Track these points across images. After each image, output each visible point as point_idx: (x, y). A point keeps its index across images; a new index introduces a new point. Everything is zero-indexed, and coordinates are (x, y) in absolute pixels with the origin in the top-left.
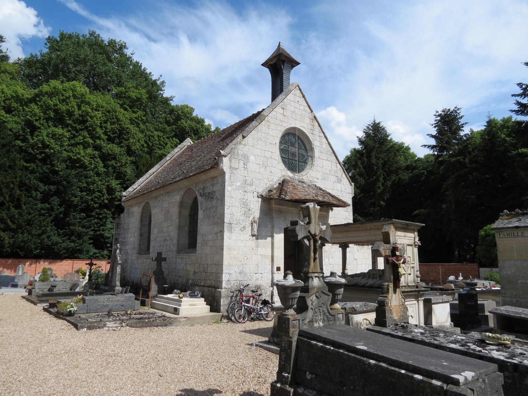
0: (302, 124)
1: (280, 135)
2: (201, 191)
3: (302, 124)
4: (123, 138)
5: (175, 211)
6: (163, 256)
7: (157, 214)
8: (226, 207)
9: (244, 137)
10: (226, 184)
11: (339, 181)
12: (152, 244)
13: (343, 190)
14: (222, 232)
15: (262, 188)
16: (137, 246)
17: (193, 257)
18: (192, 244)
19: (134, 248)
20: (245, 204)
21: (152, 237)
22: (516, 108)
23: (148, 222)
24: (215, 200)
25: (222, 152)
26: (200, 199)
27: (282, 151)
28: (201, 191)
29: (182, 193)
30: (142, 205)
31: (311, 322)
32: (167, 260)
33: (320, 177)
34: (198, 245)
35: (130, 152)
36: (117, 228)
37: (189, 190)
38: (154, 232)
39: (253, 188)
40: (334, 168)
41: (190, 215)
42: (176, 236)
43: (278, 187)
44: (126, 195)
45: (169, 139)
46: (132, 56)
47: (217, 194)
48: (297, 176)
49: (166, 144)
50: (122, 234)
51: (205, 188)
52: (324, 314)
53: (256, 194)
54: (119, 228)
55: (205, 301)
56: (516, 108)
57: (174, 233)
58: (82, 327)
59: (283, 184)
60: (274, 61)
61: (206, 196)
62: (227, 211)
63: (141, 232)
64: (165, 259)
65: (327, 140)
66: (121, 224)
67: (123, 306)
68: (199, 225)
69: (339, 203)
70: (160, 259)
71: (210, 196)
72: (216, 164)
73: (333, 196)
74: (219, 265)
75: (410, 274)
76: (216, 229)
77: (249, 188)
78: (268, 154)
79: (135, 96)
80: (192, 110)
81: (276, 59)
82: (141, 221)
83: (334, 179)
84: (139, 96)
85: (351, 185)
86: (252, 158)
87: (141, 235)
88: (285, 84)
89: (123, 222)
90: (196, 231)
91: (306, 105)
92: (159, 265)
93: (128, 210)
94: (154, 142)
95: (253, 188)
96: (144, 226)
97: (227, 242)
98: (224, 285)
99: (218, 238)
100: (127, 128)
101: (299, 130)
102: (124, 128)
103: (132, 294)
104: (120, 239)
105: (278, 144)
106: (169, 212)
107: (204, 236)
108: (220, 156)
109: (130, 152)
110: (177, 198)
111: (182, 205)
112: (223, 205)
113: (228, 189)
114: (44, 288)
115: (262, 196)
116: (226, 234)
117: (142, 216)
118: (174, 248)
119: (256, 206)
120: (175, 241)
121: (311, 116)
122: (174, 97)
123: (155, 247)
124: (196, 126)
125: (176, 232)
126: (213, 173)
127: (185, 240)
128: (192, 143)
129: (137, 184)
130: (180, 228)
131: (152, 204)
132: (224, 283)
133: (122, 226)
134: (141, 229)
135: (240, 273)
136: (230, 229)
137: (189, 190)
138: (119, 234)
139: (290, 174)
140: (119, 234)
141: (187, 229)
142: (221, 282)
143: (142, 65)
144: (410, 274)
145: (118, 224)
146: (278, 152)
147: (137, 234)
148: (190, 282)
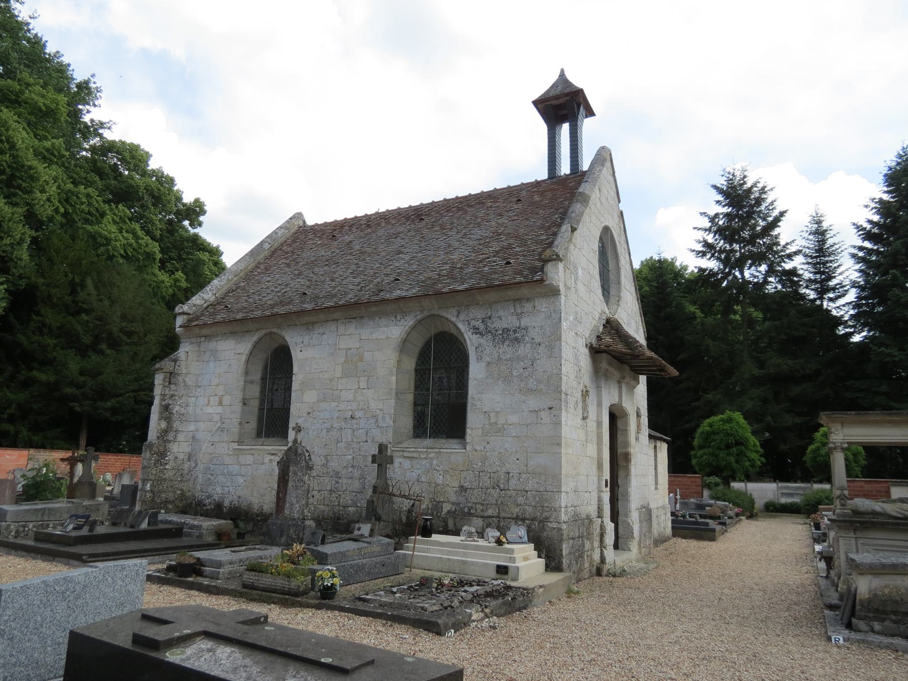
4: (19, 187)
9: (574, 230)
22: (699, 247)
24: (528, 346)
35: (31, 218)
36: (170, 383)
41: (416, 370)
44: (191, 312)
45: (110, 205)
46: (30, 21)
49: (103, 215)
50: (181, 397)
51: (490, 318)
54: (175, 384)
55: (535, 550)
56: (699, 247)
58: (447, 629)
61: (494, 336)
63: (244, 395)
65: (630, 257)
66: (178, 375)
67: (383, 565)
79: (44, 104)
80: (148, 156)
81: (568, 98)
84: (53, 106)
89: (184, 371)
94: (78, 206)
96: (252, 382)
99: (543, 421)
100: (30, 168)
102: (23, 166)
104: (177, 408)
107: (492, 415)
109: (31, 218)
114: (27, 519)
122: (115, 123)
124: (159, 190)
129: (210, 290)
133: (180, 379)
135: (575, 491)
138: (173, 396)
140: (173, 396)
143: (47, 44)
145: (171, 373)
148: (446, 508)
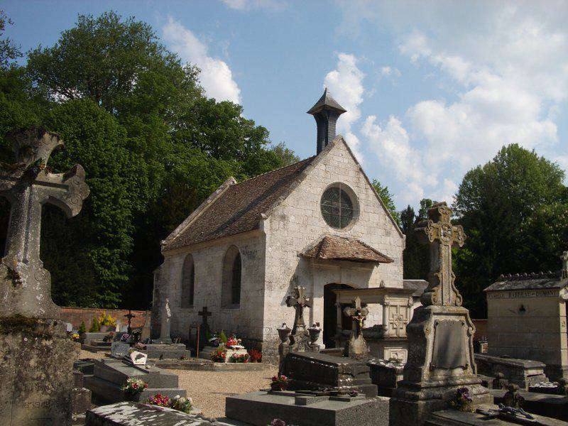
0: (346, 178)
1: (325, 186)
2: (244, 249)
3: (346, 178)
5: (218, 266)
6: (201, 310)
7: (200, 268)
8: (266, 267)
10: (267, 245)
11: (388, 234)
12: (195, 298)
13: (392, 243)
14: (263, 289)
15: (302, 247)
16: (179, 299)
17: (236, 312)
18: (236, 299)
19: (176, 301)
20: (283, 262)
21: (196, 291)
23: (190, 274)
25: (263, 215)
26: (243, 257)
27: (323, 208)
28: (244, 249)
29: (225, 248)
30: (185, 256)
31: (297, 349)
32: (493, 399)
33: (365, 232)
34: (241, 301)
37: (232, 247)
38: (198, 286)
39: (292, 248)
40: (382, 221)
41: (233, 271)
42: (220, 291)
43: (317, 246)
47: (259, 254)
48: (340, 233)
52: (305, 346)
53: (295, 254)
57: (218, 289)
59: (323, 244)
60: (319, 110)
62: (267, 271)
64: (210, 314)
68: (242, 282)
69: (382, 259)
70: (205, 313)
71: (252, 255)
72: (257, 226)
73: (377, 253)
74: (260, 320)
75: (402, 328)
76: (258, 287)
77: (290, 248)
78: (309, 213)
82: (183, 273)
83: (381, 232)
85: (402, 237)
86: (292, 218)
87: (183, 287)
88: (330, 135)
90: (240, 287)
91: (350, 157)
92: (205, 320)
93: (169, 260)
95: (292, 248)
96: (186, 278)
97: (267, 299)
98: (264, 338)
101: (343, 184)
103: (183, 345)
105: (319, 201)
106: (212, 267)
108: (260, 219)
110: (221, 253)
111: (225, 260)
112: (264, 265)
113: (268, 249)
115: (301, 255)
116: (267, 292)
117: (183, 268)
118: (218, 303)
119: (294, 263)
120: (219, 296)
121: (356, 168)
123: (199, 301)
125: (220, 287)
126: (255, 233)
127: (229, 296)
128: (236, 182)
130: (224, 283)
131: (195, 257)
132: (264, 336)
134: (183, 281)
136: (271, 288)
137: (232, 247)
139: (332, 231)
141: (230, 284)
142: (262, 335)
144: (402, 328)
146: (319, 210)
147: (179, 286)
